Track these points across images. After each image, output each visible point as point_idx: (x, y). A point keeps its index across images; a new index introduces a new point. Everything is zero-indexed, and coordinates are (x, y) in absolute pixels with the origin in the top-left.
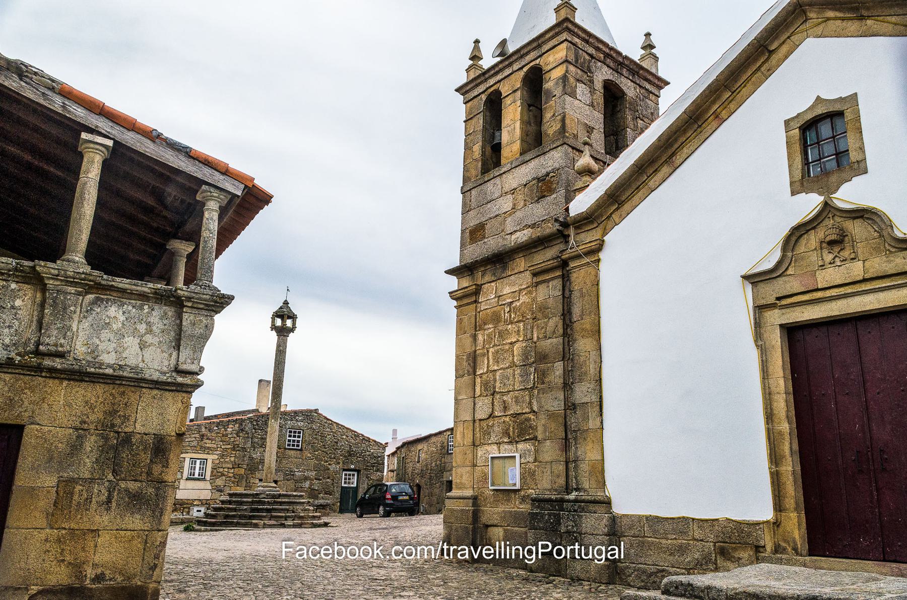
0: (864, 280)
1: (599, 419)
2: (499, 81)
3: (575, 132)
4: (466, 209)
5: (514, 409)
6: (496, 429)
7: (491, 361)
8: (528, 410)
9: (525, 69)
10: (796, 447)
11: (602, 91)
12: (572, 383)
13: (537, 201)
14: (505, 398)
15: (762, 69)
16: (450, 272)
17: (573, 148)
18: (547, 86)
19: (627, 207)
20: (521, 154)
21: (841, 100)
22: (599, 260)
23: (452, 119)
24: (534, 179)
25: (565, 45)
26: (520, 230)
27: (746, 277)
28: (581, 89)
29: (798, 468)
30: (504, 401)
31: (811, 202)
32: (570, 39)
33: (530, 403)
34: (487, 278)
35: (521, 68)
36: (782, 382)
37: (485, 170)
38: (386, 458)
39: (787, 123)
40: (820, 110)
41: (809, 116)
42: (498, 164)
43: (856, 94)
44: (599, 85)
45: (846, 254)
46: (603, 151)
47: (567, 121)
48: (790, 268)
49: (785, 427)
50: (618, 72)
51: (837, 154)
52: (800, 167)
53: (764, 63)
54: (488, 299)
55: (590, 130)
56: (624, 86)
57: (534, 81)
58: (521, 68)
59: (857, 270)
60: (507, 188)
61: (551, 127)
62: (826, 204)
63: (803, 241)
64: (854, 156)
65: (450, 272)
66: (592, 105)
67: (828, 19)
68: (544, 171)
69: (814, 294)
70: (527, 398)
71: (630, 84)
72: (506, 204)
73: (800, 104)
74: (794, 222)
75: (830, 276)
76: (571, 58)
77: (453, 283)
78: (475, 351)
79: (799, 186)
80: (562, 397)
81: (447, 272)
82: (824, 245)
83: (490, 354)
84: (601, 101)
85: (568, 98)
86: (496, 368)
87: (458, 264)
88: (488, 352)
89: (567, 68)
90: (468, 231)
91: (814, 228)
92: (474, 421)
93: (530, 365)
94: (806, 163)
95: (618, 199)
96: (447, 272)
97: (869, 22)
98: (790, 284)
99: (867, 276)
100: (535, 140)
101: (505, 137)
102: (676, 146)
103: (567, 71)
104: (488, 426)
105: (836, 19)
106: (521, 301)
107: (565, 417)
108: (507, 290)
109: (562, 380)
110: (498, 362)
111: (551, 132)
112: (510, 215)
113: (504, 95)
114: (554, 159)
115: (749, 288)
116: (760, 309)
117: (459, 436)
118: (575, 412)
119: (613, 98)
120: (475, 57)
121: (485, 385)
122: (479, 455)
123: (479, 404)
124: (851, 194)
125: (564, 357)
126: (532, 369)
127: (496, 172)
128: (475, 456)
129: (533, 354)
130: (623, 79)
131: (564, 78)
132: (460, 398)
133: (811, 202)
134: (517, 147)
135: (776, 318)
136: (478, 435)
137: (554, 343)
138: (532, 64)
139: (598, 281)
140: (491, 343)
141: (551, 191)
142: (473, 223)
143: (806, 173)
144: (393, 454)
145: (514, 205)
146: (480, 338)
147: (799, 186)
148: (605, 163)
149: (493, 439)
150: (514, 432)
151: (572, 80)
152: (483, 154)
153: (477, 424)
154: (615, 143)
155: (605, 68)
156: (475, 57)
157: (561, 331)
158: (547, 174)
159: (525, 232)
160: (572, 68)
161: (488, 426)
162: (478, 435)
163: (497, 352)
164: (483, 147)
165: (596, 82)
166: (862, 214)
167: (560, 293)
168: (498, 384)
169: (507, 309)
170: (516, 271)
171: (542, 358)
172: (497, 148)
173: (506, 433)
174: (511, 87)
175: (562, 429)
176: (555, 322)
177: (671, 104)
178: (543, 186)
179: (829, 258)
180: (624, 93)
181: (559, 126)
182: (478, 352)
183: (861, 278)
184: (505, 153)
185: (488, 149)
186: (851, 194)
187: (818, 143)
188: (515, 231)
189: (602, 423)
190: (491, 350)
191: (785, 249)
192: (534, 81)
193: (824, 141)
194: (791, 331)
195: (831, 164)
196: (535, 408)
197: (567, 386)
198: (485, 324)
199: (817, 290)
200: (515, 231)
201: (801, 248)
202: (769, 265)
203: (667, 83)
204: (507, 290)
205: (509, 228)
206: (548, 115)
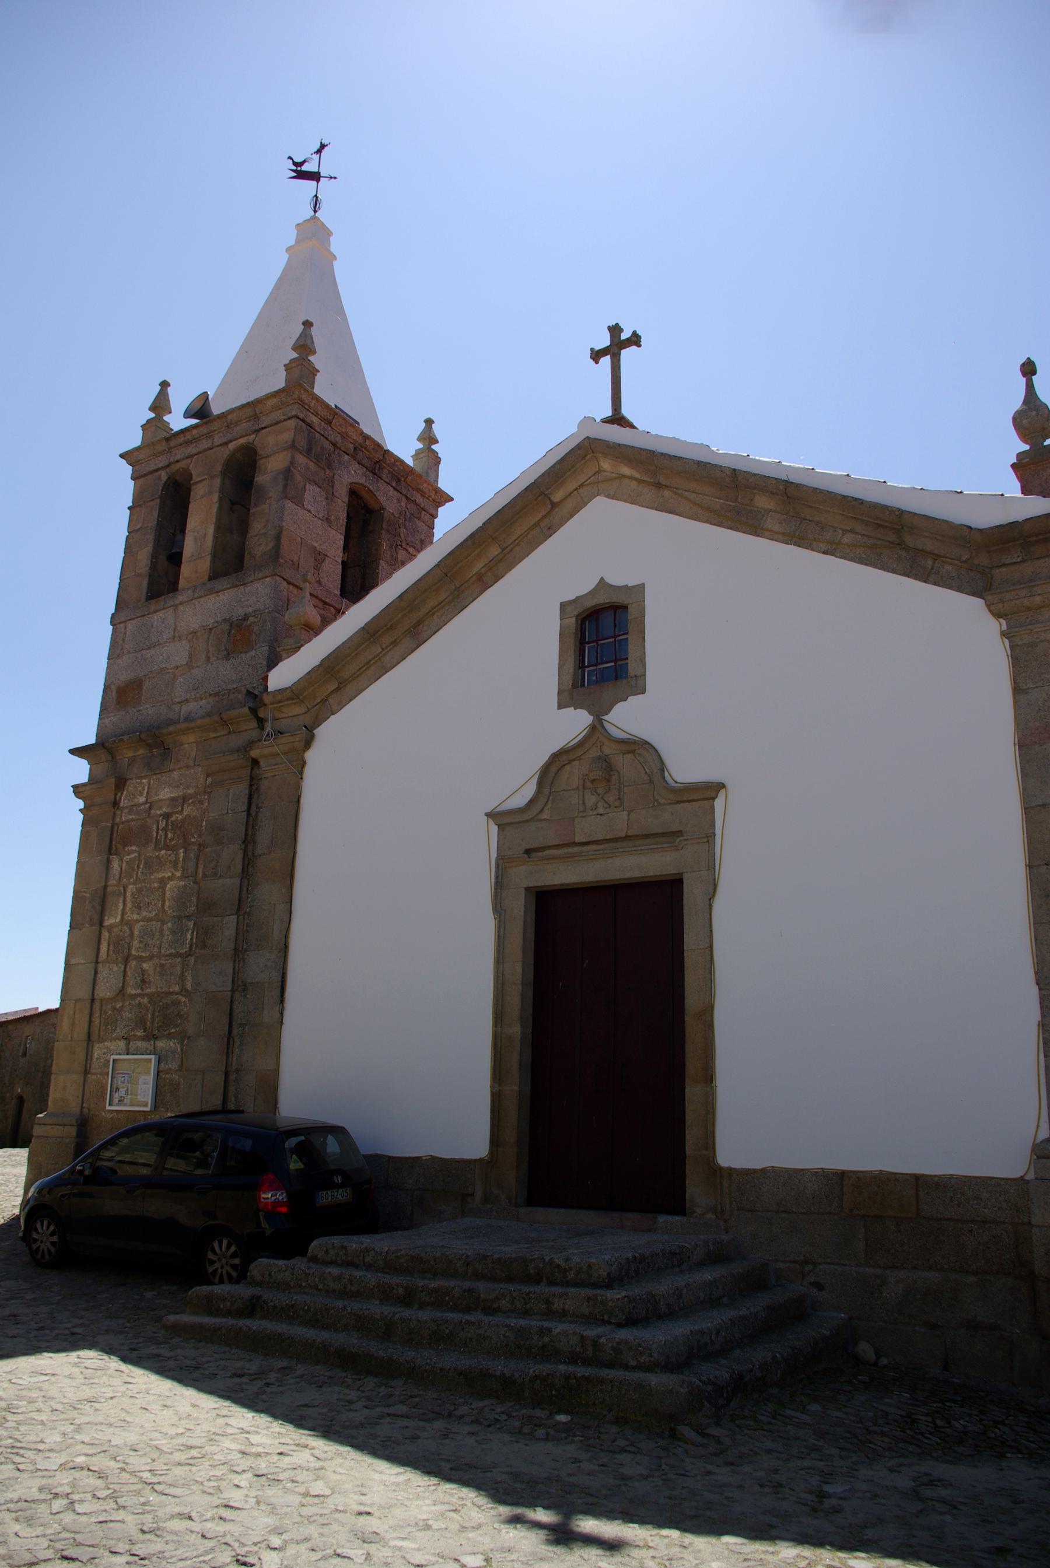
1: (277, 1008)
2: (191, 456)
3: (296, 559)
5: (157, 984)
6: (127, 1015)
7: (129, 905)
8: (177, 989)
9: (232, 446)
11: (346, 499)
12: (246, 951)
13: (228, 656)
14: (145, 966)
15: (542, 524)
16: (76, 752)
17: (289, 583)
20: (210, 579)
21: (626, 588)
24: (225, 620)
25: (292, 423)
28: (312, 492)
30: (143, 971)
31: (575, 723)
32: (301, 416)
33: (182, 978)
35: (226, 444)
36: (519, 969)
39: (564, 606)
40: (602, 599)
42: (173, 587)
43: (643, 585)
45: (611, 798)
46: (338, 592)
47: (284, 541)
48: (546, 811)
49: (516, 1030)
50: (375, 474)
52: (571, 670)
53: (544, 517)
55: (319, 558)
56: (377, 502)
59: (619, 822)
61: (258, 545)
62: (597, 728)
65: (76, 752)
66: (328, 520)
67: (624, 476)
68: (241, 612)
69: (570, 847)
70: (179, 969)
71: (392, 492)
73: (578, 585)
74: (556, 747)
75: (589, 827)
78: (106, 887)
79: (568, 698)
80: (231, 970)
81: (74, 752)
82: (588, 784)
83: (129, 894)
84: (343, 515)
85: (289, 504)
86: (135, 917)
88: (125, 891)
89: (293, 457)
90: (114, 688)
92: (93, 1000)
93: (188, 918)
95: (340, 680)
96: (74, 752)
97: (667, 493)
99: (630, 833)
100: (230, 562)
101: (189, 547)
102: (424, 610)
103: (292, 463)
104: (114, 1008)
105: (631, 478)
106: (185, 813)
107: (232, 1002)
109: (232, 946)
110: (139, 908)
113: (195, 479)
114: (256, 594)
115: (494, 829)
117: (65, 1024)
118: (245, 996)
121: (116, 944)
122: (96, 1055)
123: (104, 972)
124: (628, 717)
125: (238, 909)
126: (191, 924)
128: (88, 1056)
129: (194, 899)
130: (382, 485)
131: (287, 473)
132: (73, 961)
133: (575, 723)
134: (205, 565)
136: (97, 1022)
137: (226, 885)
139: (299, 797)
140: (131, 876)
142: (124, 677)
143: (578, 683)
146: (115, 865)
147: (568, 698)
149: (120, 1031)
150: (153, 1022)
151: (298, 477)
152: (153, 566)
153: (97, 1005)
154: (357, 582)
155: (355, 466)
156: (160, 405)
157: (239, 868)
158: (246, 617)
159: (203, 702)
160: (301, 459)
161: (114, 1008)
162: (97, 1022)
164: (154, 556)
165: (337, 485)
166: (636, 747)
167: (245, 808)
168: (136, 943)
169: (162, 824)
171: (207, 906)
172: (175, 559)
173: (141, 1022)
175: (225, 1020)
176: (231, 854)
177: (449, 524)
179: (591, 799)
181: (271, 545)
182: (109, 889)
183: (623, 834)
184: (186, 570)
186: (628, 717)
188: (187, 701)
189: (282, 1014)
190: (131, 888)
191: (540, 783)
193: (602, 642)
194: (546, 902)
196: (189, 986)
197: (238, 954)
199: (575, 844)
202: (521, 800)
204: (166, 793)
205: (179, 694)
206: (257, 527)
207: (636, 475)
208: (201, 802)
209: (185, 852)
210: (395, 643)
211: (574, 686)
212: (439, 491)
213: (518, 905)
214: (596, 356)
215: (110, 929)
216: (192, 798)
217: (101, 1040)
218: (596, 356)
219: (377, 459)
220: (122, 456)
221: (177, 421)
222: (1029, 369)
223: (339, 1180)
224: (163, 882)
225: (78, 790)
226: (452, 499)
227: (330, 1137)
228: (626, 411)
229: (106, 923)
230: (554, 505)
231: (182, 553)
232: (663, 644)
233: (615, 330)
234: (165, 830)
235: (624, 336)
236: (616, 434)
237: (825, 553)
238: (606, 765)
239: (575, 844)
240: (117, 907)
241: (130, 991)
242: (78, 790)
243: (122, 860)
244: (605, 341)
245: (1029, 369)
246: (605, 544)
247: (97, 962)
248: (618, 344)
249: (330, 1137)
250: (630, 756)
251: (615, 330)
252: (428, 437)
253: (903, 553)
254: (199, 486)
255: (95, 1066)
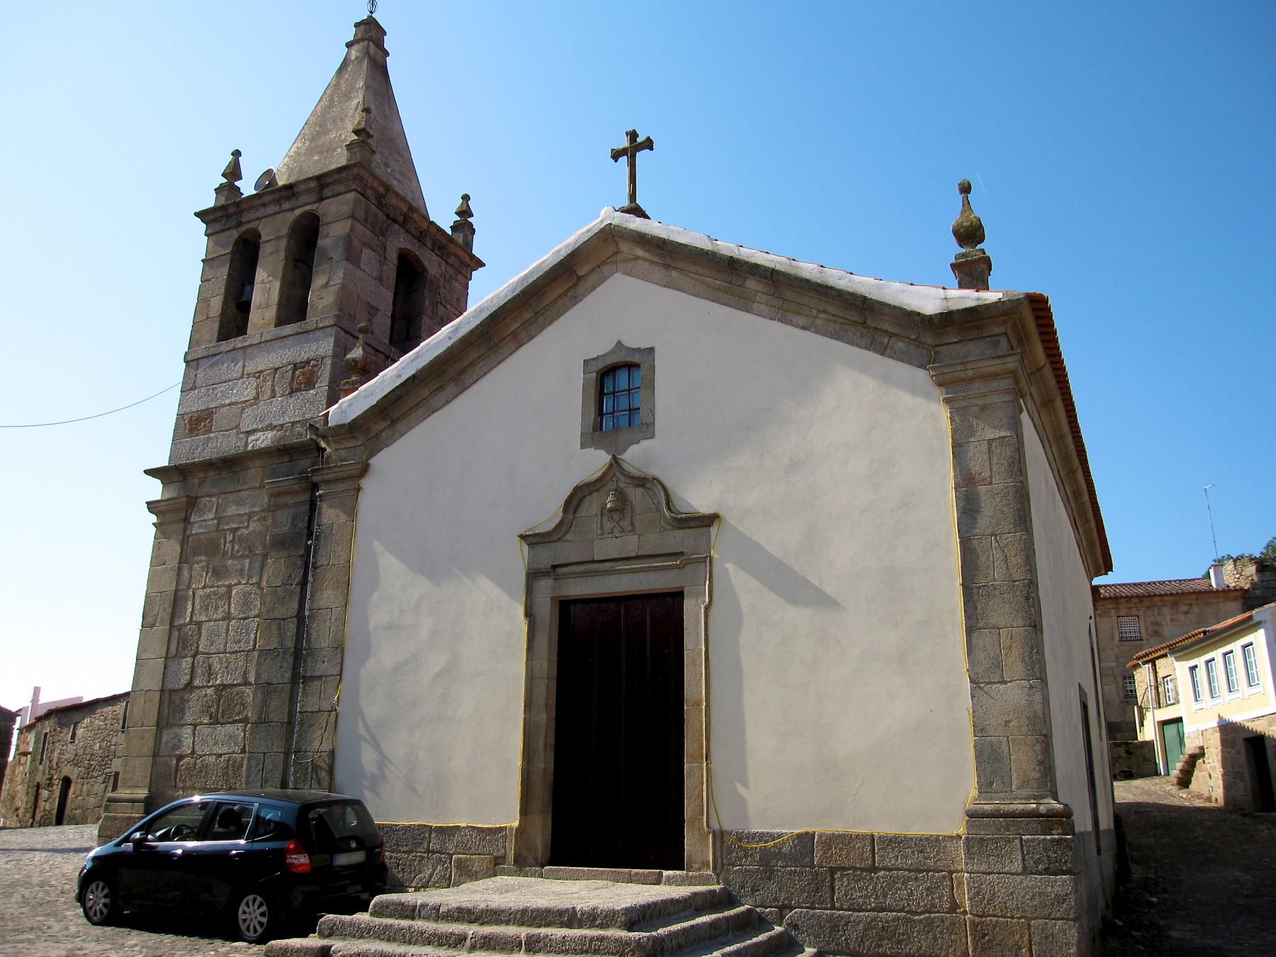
0: (637, 557)
2: (259, 219)
3: (352, 312)
4: (188, 387)
9: (298, 212)
10: (552, 740)
16: (151, 472)
17: (346, 332)
18: (321, 242)
19: (400, 427)
21: (639, 350)
22: (359, 489)
23: (187, 252)
26: (263, 430)
27: (522, 537)
28: (367, 256)
29: (551, 766)
31: (598, 460)
34: (207, 488)
36: (545, 665)
37: (224, 335)
38: (16, 733)
41: (609, 361)
42: (242, 329)
44: (393, 256)
45: (626, 524)
46: (387, 342)
51: (630, 410)
54: (203, 523)
55: (373, 310)
56: (422, 266)
57: (305, 242)
58: (292, 210)
59: (631, 544)
60: (249, 369)
62: (615, 463)
63: (586, 503)
64: (643, 415)
65: (151, 472)
66: (380, 279)
67: (638, 258)
69: (593, 567)
72: (246, 391)
73: (600, 346)
75: (606, 547)
76: (361, 214)
77: (155, 489)
84: (393, 275)
86: (203, 618)
87: (165, 463)
91: (598, 490)
92: (162, 691)
94: (600, 413)
95: (394, 413)
97: (674, 273)
98: (569, 551)
99: (641, 553)
101: (257, 297)
102: (467, 362)
103: (351, 230)
105: (645, 259)
108: (232, 510)
111: (320, 304)
112: (252, 405)
113: (264, 238)
116: (533, 576)
119: (409, 275)
120: (233, 172)
122: (164, 740)
124: (636, 456)
127: (238, 342)
133: (598, 460)
134: (272, 313)
135: (545, 587)
136: (166, 711)
138: (307, 208)
141: (310, 383)
142: (197, 406)
143: (598, 427)
144: (29, 728)
145: (258, 394)
148: (388, 357)
151: (355, 243)
156: (233, 172)
160: (359, 227)
162: (166, 711)
163: (208, 596)
166: (643, 482)
169: (230, 538)
170: (247, 486)
172: (244, 307)
174: (275, 236)
177: (486, 291)
178: (302, 376)
179: (608, 525)
180: (424, 270)
183: (634, 554)
184: (254, 316)
185: (232, 306)
186: (636, 456)
187: (614, 393)
188: (254, 431)
191: (566, 510)
192: (305, 242)
193: (617, 390)
194: (565, 607)
195: (624, 421)
198: (195, 554)
199: (593, 562)
200: (254, 431)
201: (583, 512)
202: (550, 527)
203: (484, 265)
207: (648, 256)
208: (265, 519)
209: (250, 563)
210: (441, 388)
211: (595, 430)
212: (473, 257)
213: (545, 609)
214: (616, 155)
215: (180, 628)
216: (255, 512)
217: (169, 726)
218: (616, 155)
219: (427, 232)
220: (197, 214)
221: (247, 187)
222: (966, 189)
223: (354, 845)
224: (230, 587)
225: (152, 506)
226: (484, 265)
227: (349, 809)
228: (640, 201)
229: (176, 624)
230: (579, 278)
231: (250, 302)
232: (669, 394)
233: (633, 135)
234: (232, 542)
235: (639, 140)
236: (635, 223)
237: (803, 328)
238: (621, 497)
239: (593, 562)
240: (186, 608)
241: (197, 683)
242: (152, 506)
243: (191, 568)
244: (624, 143)
245: (966, 189)
246: (623, 311)
247: (166, 658)
248: (635, 146)
249: (349, 809)
250: (641, 489)
251: (633, 135)
252: (465, 213)
253: (865, 331)
254: (268, 245)
255: (164, 750)
